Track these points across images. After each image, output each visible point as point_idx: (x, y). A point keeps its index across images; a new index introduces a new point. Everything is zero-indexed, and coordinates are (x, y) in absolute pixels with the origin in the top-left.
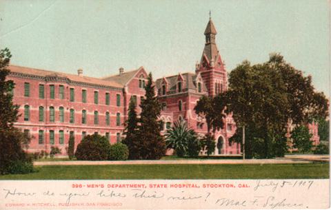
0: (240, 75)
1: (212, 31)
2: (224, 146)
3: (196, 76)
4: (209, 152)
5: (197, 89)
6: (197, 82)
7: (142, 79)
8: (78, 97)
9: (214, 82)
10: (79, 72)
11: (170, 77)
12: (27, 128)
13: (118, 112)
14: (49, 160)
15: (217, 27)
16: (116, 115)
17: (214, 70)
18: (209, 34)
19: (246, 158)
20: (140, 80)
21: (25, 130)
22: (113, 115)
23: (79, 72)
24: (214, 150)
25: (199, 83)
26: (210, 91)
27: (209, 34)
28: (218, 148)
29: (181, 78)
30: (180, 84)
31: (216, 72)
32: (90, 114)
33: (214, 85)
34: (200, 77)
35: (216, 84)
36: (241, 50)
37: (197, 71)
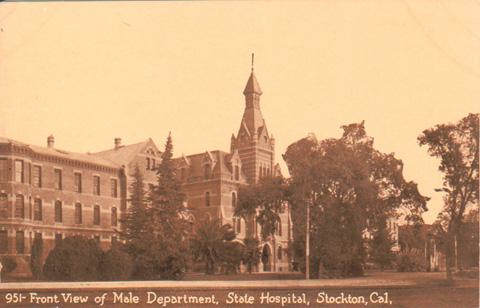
0: (300, 152)
1: (256, 89)
2: (272, 258)
3: (232, 155)
4: (250, 269)
5: (234, 175)
6: (234, 165)
7: (151, 157)
8: (67, 181)
9: (258, 166)
10: (50, 140)
11: (190, 157)
12: (295, 272)
13: (110, 204)
14: (100, 292)
15: (261, 82)
16: (73, 207)
17: (256, 147)
18: (250, 92)
19: (311, 278)
20: (148, 159)
21: (297, 270)
22: (106, 211)
23: (50, 140)
24: (256, 264)
25: (237, 167)
26: (250, 179)
27: (250, 92)
28: (263, 261)
29: (209, 157)
30: (207, 166)
31: (260, 150)
32: (49, 206)
33: (258, 170)
34: (238, 157)
35: (261, 168)
36: (297, 119)
37: (233, 148)
